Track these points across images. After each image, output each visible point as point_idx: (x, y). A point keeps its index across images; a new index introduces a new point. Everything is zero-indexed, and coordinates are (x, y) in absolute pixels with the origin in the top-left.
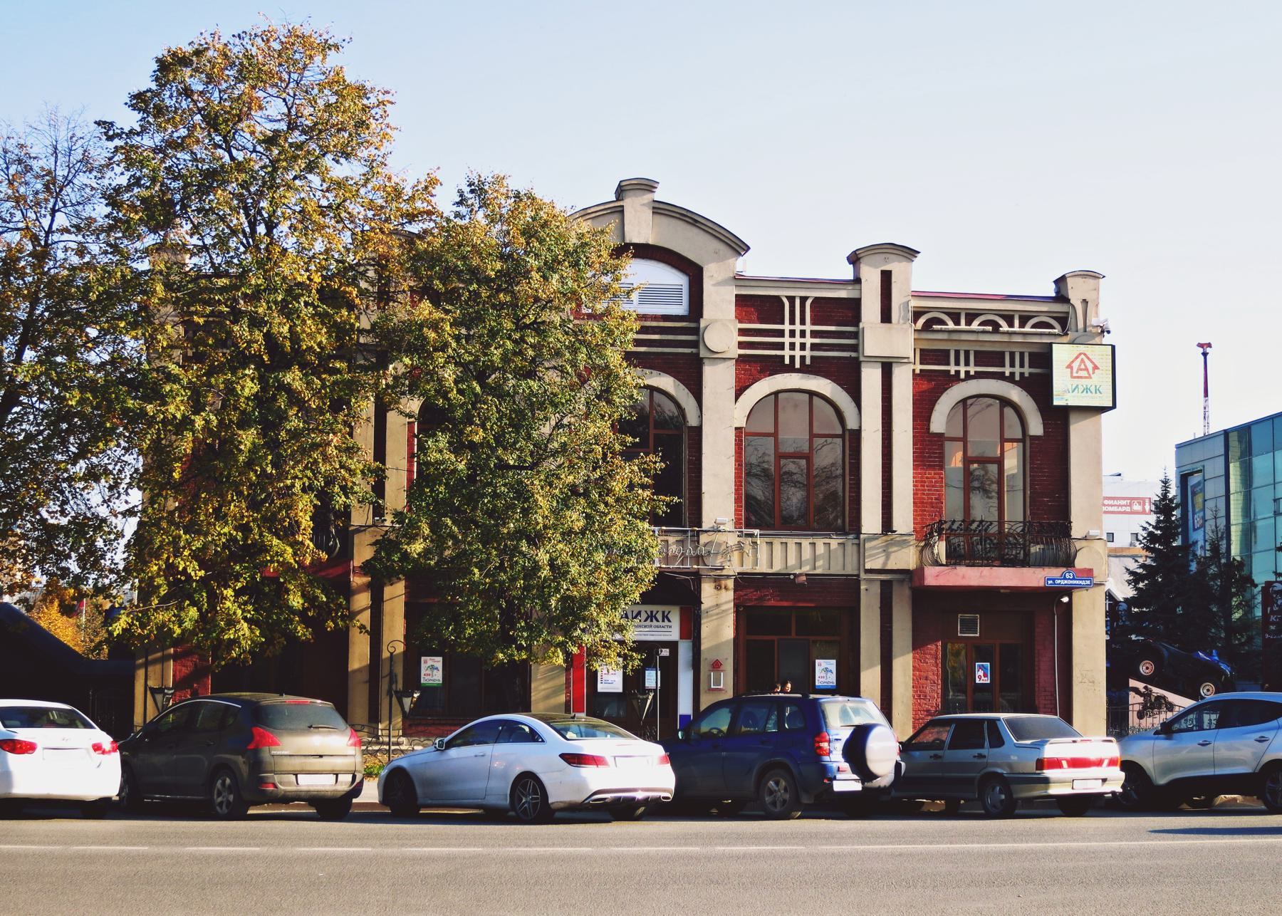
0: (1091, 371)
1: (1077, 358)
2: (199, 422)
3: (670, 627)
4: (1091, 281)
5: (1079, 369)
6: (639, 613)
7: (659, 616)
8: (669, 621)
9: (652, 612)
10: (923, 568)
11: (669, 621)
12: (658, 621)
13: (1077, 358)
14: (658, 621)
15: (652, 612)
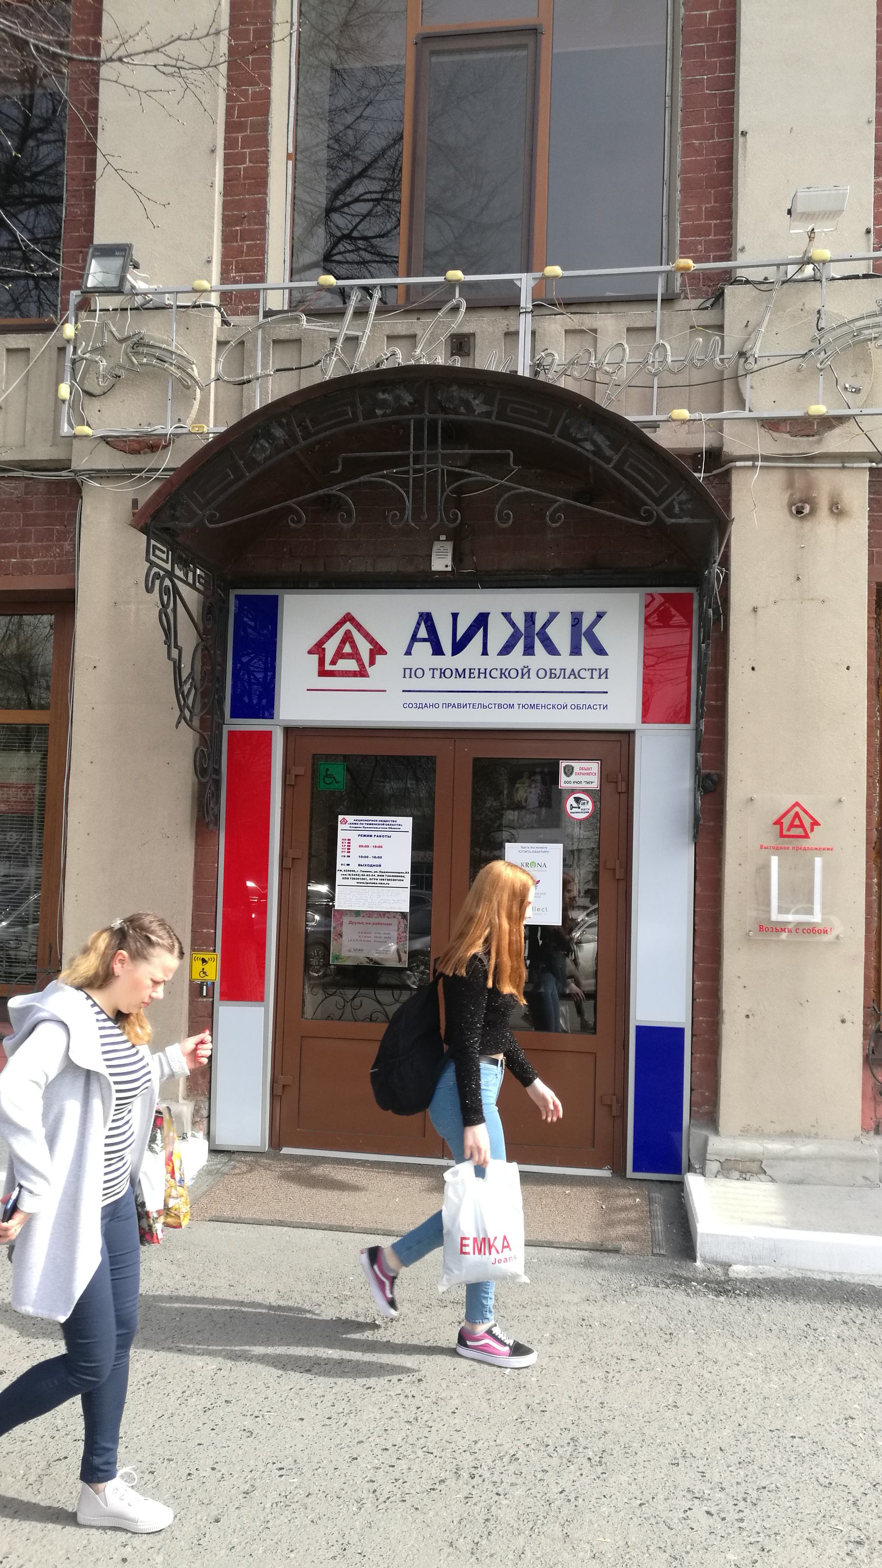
0: (366, 658)
3: (604, 674)
5: (339, 655)
6: (482, 621)
7: (560, 634)
8: (600, 650)
9: (530, 617)
10: (271, 1145)
11: (600, 650)
12: (552, 649)
14: (552, 649)
15: (530, 617)
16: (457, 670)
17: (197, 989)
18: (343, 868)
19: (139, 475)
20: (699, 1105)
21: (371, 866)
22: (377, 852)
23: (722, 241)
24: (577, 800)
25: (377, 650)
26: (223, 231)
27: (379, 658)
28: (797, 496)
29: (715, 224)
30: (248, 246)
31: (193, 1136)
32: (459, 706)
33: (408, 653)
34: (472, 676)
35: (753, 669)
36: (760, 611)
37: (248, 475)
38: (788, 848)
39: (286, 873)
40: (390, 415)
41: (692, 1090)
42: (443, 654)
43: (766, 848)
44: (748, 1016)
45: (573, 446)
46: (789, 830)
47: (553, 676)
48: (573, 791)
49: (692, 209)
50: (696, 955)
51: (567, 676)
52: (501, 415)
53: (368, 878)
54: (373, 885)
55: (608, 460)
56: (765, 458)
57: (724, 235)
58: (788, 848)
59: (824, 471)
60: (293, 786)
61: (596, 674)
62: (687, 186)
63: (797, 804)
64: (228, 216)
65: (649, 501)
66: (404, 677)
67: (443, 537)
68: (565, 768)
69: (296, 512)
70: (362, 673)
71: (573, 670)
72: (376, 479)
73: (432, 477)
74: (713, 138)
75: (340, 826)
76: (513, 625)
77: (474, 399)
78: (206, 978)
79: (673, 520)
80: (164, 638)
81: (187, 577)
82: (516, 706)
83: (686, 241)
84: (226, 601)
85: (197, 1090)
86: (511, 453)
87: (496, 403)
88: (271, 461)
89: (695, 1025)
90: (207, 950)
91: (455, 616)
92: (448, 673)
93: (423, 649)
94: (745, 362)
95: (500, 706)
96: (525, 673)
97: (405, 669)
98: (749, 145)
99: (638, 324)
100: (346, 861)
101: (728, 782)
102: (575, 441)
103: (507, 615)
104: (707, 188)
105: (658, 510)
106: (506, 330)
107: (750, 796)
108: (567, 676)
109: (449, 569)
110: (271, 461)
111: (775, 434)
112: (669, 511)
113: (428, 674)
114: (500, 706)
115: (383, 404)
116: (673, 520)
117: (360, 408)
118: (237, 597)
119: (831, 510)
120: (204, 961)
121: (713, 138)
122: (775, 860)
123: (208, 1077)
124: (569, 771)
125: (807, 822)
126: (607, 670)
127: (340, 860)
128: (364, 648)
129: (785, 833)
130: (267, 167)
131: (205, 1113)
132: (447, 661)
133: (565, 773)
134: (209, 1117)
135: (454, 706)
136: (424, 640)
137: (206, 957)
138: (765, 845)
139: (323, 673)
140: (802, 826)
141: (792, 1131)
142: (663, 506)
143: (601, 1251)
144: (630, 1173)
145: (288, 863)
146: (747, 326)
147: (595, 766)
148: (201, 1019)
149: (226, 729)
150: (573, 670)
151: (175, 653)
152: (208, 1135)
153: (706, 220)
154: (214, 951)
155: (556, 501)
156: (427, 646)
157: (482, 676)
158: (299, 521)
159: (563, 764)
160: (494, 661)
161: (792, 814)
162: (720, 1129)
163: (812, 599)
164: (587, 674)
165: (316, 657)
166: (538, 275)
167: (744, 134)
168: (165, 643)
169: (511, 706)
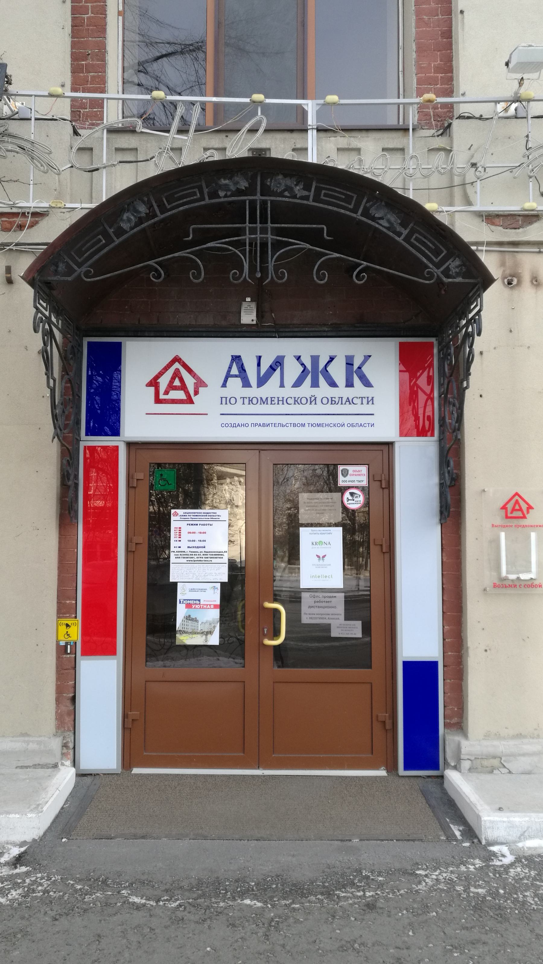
1: (166, 368)
2: (181, 926)
3: (371, 401)
4: (325, 126)
5: (171, 387)
6: (278, 363)
8: (367, 383)
9: (315, 359)
11: (367, 383)
12: (333, 384)
13: (166, 368)
14: (333, 384)
15: (315, 359)
16: (261, 398)
17: (62, 650)
18: (176, 550)
19: (8, 248)
20: (451, 718)
21: (198, 547)
22: (202, 537)
23: (446, 89)
24: (352, 494)
25: (200, 383)
26: (72, 64)
27: (201, 389)
28: (508, 272)
29: (441, 77)
30: (93, 77)
31: (63, 764)
32: (264, 425)
33: (224, 385)
34: (273, 403)
35: (481, 396)
36: (484, 353)
37: (117, 241)
38: (511, 526)
39: (131, 555)
40: (231, 196)
41: (445, 707)
42: (251, 387)
43: (497, 526)
44: (486, 651)
45: (373, 223)
46: (512, 513)
47: (333, 402)
48: (349, 488)
49: (425, 65)
50: (445, 607)
51: (344, 402)
52: (317, 199)
53: (195, 557)
54: (200, 562)
55: (399, 234)
56: (489, 244)
57: (448, 85)
58: (511, 526)
59: (526, 254)
60: (135, 488)
61: (365, 401)
62: (420, 50)
63: (517, 494)
64: (75, 53)
65: (431, 266)
66: (222, 404)
67: (248, 299)
68: (342, 471)
69: (156, 270)
70: (190, 401)
71: (348, 398)
72: (220, 245)
73: (264, 245)
74: (438, 15)
75: (173, 518)
76: (303, 364)
77: (296, 185)
78: (70, 639)
79: (450, 280)
80: (45, 370)
81: (58, 324)
82: (307, 425)
83: (420, 88)
84: (81, 345)
85: (64, 727)
86: (325, 228)
87: (313, 189)
88: (135, 230)
89: (446, 658)
90: (69, 617)
91: (259, 358)
92: (255, 401)
93: (235, 383)
94: (476, 170)
95: (295, 425)
96: (312, 400)
97: (222, 398)
98: (465, 21)
99: (391, 146)
100: (178, 544)
101: (467, 479)
102: (374, 219)
103: (298, 358)
104: (434, 50)
105: (438, 272)
106: (293, 147)
107: (483, 489)
108: (344, 403)
109: (255, 322)
110: (135, 230)
111: (493, 227)
112: (447, 273)
113: (240, 401)
114: (295, 425)
115: (226, 188)
116: (450, 280)
117: (206, 191)
118: (89, 344)
119: (532, 282)
120: (67, 625)
121: (438, 15)
122: (503, 535)
123: (73, 716)
124: (345, 473)
125: (524, 507)
126: (373, 398)
127: (173, 544)
128: (190, 382)
129: (509, 515)
130: (105, 18)
131: (71, 745)
132: (254, 392)
133: (342, 475)
134: (74, 748)
135: (260, 425)
136: (236, 376)
137: (69, 623)
138: (495, 524)
139: (158, 400)
140: (520, 509)
141: (521, 734)
142: (442, 269)
143: (408, 840)
144: (401, 771)
145: (133, 547)
146: (469, 149)
147: (364, 469)
148: (66, 671)
149: (82, 445)
150: (348, 398)
151: (51, 381)
152: (74, 763)
153: (434, 73)
154: (76, 617)
155: (361, 264)
156: (238, 381)
157: (281, 402)
158: (159, 276)
159: (341, 468)
160: (289, 392)
161: (514, 500)
162: (470, 735)
163: (521, 346)
164: (358, 401)
165: (152, 389)
166: (321, 102)
167: (462, 12)
168: (46, 374)
169: (303, 425)
